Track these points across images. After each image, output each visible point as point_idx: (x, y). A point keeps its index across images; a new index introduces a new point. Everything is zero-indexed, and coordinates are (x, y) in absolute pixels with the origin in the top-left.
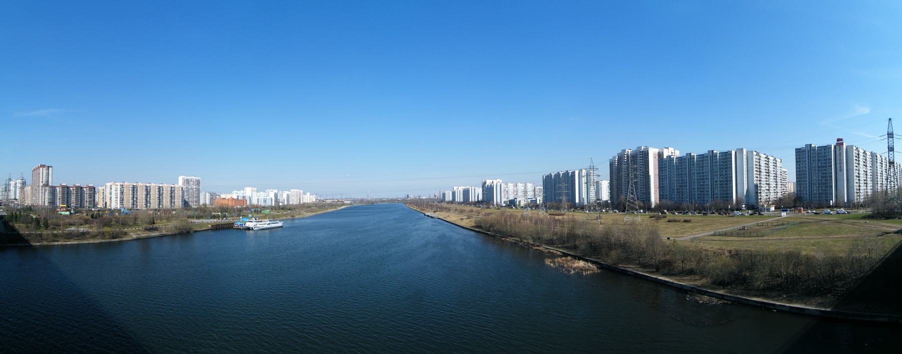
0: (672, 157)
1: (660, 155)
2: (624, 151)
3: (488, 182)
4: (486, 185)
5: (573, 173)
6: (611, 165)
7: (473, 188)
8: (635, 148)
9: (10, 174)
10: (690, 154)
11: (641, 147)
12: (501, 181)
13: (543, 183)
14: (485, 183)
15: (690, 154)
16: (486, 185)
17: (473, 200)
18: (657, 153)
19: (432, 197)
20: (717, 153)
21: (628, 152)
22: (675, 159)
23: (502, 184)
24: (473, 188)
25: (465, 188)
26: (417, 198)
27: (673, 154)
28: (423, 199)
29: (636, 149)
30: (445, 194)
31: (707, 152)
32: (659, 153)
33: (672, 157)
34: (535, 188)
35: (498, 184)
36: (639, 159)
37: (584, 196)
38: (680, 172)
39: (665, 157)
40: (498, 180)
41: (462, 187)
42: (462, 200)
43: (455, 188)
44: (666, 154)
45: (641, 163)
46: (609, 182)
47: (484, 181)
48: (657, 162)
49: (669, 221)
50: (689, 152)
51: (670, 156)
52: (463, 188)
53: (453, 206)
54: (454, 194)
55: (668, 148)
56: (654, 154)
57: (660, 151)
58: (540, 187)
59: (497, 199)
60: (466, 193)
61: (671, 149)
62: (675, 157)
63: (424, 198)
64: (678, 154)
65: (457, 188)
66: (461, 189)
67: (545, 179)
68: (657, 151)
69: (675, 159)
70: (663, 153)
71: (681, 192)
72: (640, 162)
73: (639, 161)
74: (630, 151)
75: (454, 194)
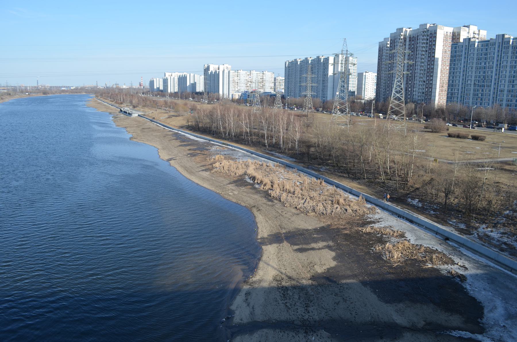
0: (472, 40)
1: (455, 36)
2: (401, 30)
3: (212, 69)
4: (209, 72)
5: (327, 60)
6: (381, 50)
7: (192, 75)
8: (416, 27)
9: (37, 81)
10: (503, 35)
11: (426, 25)
12: (230, 67)
13: (285, 70)
14: (208, 68)
15: (503, 35)
16: (209, 72)
17: (172, 91)
18: (450, 35)
19: (136, 86)
20: (510, 38)
21: (406, 31)
22: (511, 41)
23: (231, 71)
24: (192, 75)
25: (181, 74)
26: (115, 87)
27: (476, 36)
28: (122, 89)
29: (418, 27)
30: (153, 81)
31: (494, 37)
32: (454, 34)
33: (472, 40)
34: (275, 79)
35: (226, 72)
36: (421, 45)
37: (226, 92)
38: (483, 64)
39: (461, 40)
40: (226, 65)
41: (176, 73)
42: (176, 90)
43: (167, 75)
44: (464, 35)
45: (424, 49)
46: (376, 74)
47: (206, 66)
48: (449, 49)
49: (450, 136)
50: (501, 33)
51: (469, 39)
52: (179, 74)
53: (161, 100)
54: (165, 81)
55: (468, 27)
56: (446, 36)
57: (456, 31)
58: (281, 78)
59: (223, 90)
60: (182, 80)
61: (474, 28)
62: (477, 41)
63: (124, 87)
64: (484, 35)
65: (170, 74)
66: (176, 75)
67: (289, 67)
68: (450, 30)
69: (511, 41)
70: (459, 35)
71: (480, 95)
72: (422, 47)
73: (421, 45)
74: (408, 30)
75: (165, 81)
